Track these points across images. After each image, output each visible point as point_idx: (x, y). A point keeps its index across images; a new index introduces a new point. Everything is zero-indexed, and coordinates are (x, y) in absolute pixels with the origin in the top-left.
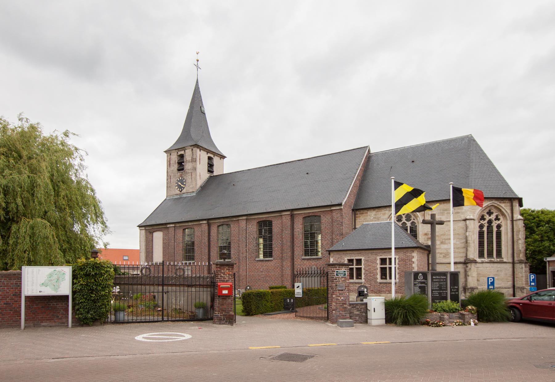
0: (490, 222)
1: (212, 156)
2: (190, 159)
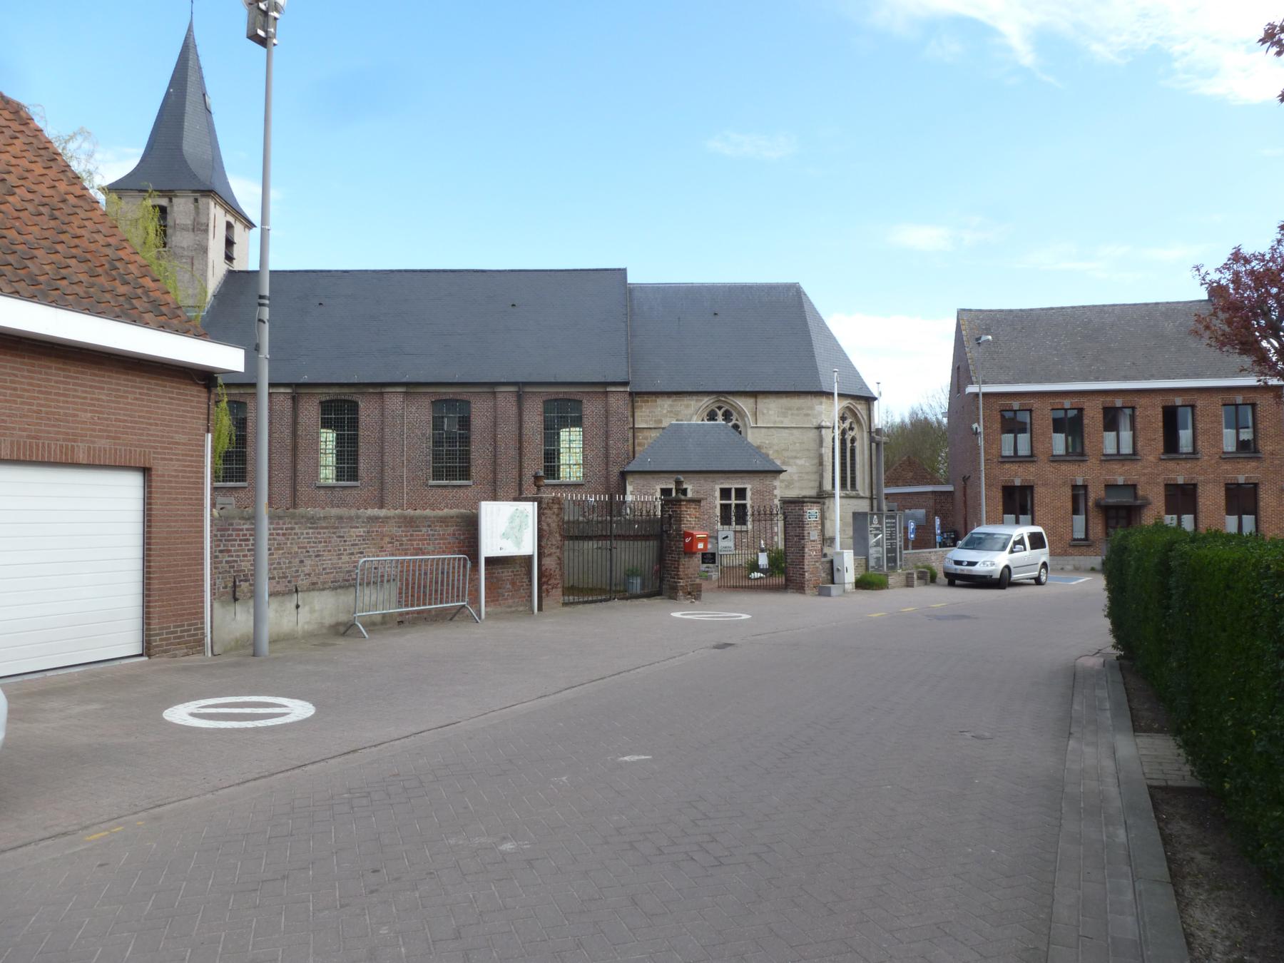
0: (843, 433)
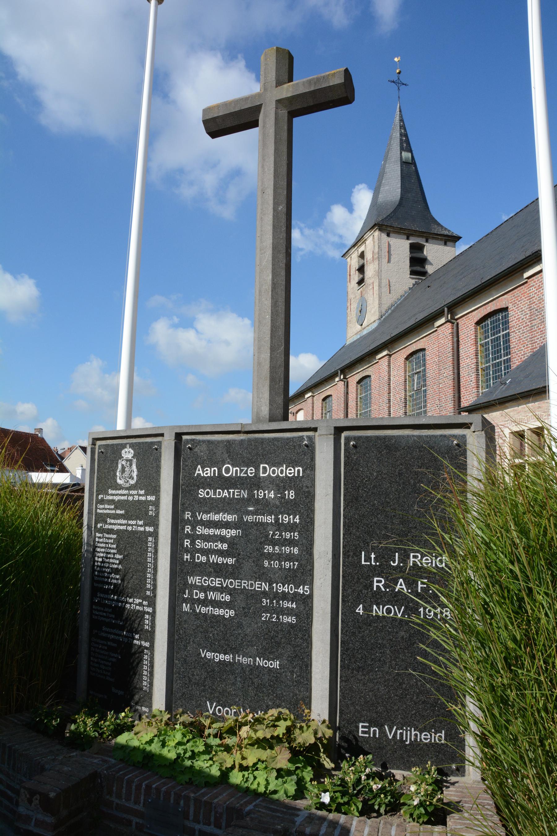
1: (421, 241)
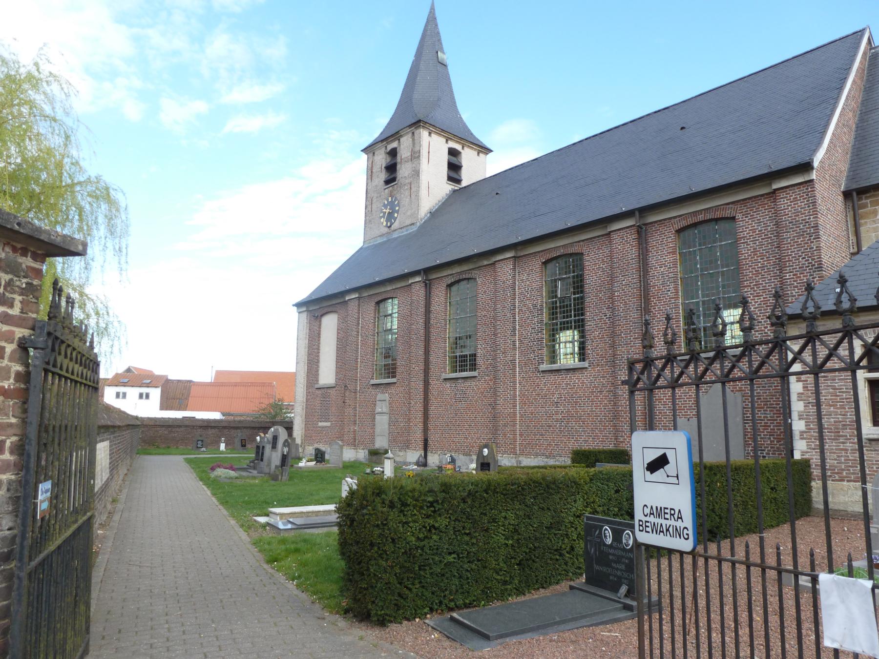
1: (458, 147)
2: (409, 154)
